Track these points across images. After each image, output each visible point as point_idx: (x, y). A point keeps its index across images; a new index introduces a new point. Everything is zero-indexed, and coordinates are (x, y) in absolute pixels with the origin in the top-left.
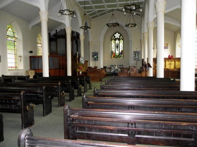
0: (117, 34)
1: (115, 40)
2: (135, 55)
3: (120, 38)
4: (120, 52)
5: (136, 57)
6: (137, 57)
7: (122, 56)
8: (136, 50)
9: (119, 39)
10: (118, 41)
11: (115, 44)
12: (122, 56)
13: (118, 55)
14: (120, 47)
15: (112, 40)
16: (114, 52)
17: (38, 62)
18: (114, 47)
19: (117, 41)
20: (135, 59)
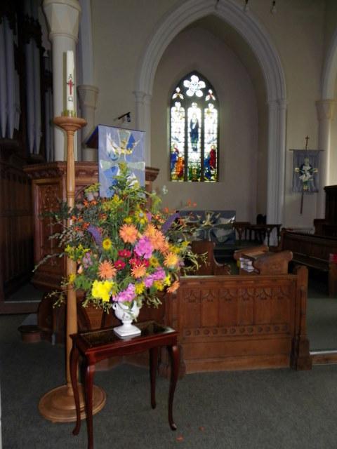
0: (194, 78)
1: (186, 103)
2: (301, 168)
3: (207, 98)
4: (206, 157)
5: (304, 178)
6: (306, 177)
7: (213, 172)
8: (301, 147)
9: (203, 104)
10: (198, 111)
11: (186, 123)
12: (213, 172)
13: (198, 171)
14: (208, 138)
15: (172, 104)
16: (181, 155)
17: (43, 92)
18: (183, 134)
19: (194, 112)
20: (298, 183)
